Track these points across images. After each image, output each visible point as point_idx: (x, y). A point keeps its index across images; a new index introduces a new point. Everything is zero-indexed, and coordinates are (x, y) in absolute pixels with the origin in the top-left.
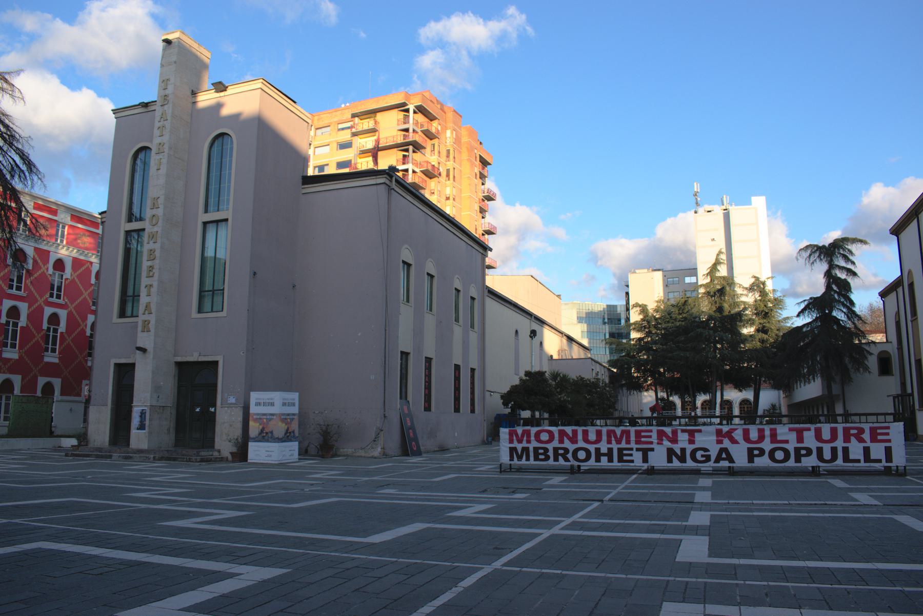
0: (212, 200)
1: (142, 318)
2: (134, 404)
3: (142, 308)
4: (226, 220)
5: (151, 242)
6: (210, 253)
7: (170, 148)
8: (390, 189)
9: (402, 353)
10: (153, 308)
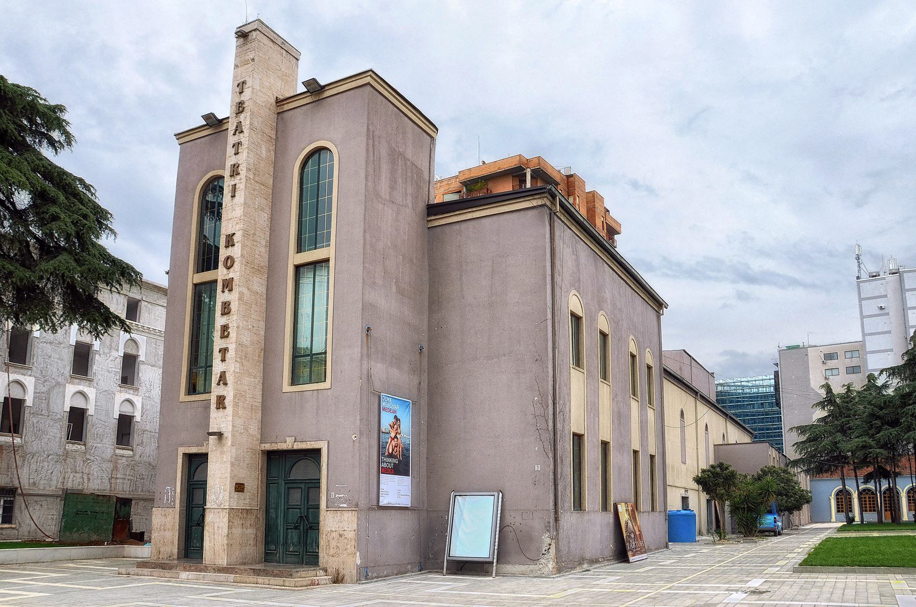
0: (306, 236)
1: (217, 390)
2: (208, 505)
3: (215, 379)
4: (327, 261)
5: (226, 291)
6: (303, 343)
7: (248, 170)
8: (552, 214)
9: (574, 434)
10: (230, 378)
